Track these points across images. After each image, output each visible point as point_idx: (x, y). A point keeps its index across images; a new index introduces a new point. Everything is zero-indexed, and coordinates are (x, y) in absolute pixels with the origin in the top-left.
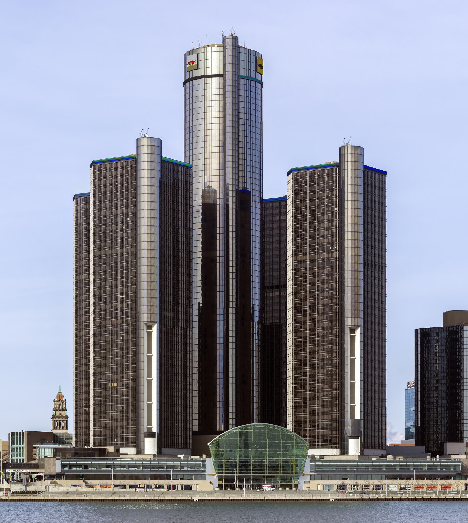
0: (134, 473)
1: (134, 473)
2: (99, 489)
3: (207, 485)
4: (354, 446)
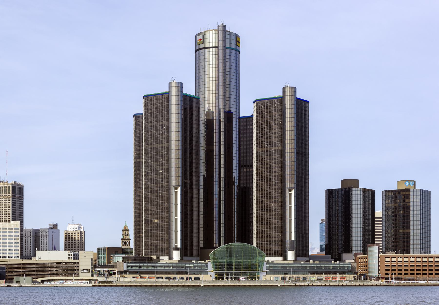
0: (167, 271)
1: (167, 271)
2: (148, 280)
3: (208, 277)
4: (291, 255)
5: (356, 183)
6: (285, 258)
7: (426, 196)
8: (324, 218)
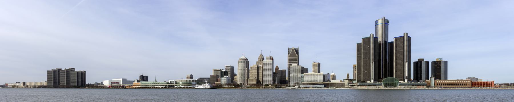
0: (370, 85)
1: (370, 85)
2: (364, 87)
3: (382, 87)
4: (406, 81)
5: (423, 59)
6: (404, 81)
7: (446, 63)
8: (354, 61)
